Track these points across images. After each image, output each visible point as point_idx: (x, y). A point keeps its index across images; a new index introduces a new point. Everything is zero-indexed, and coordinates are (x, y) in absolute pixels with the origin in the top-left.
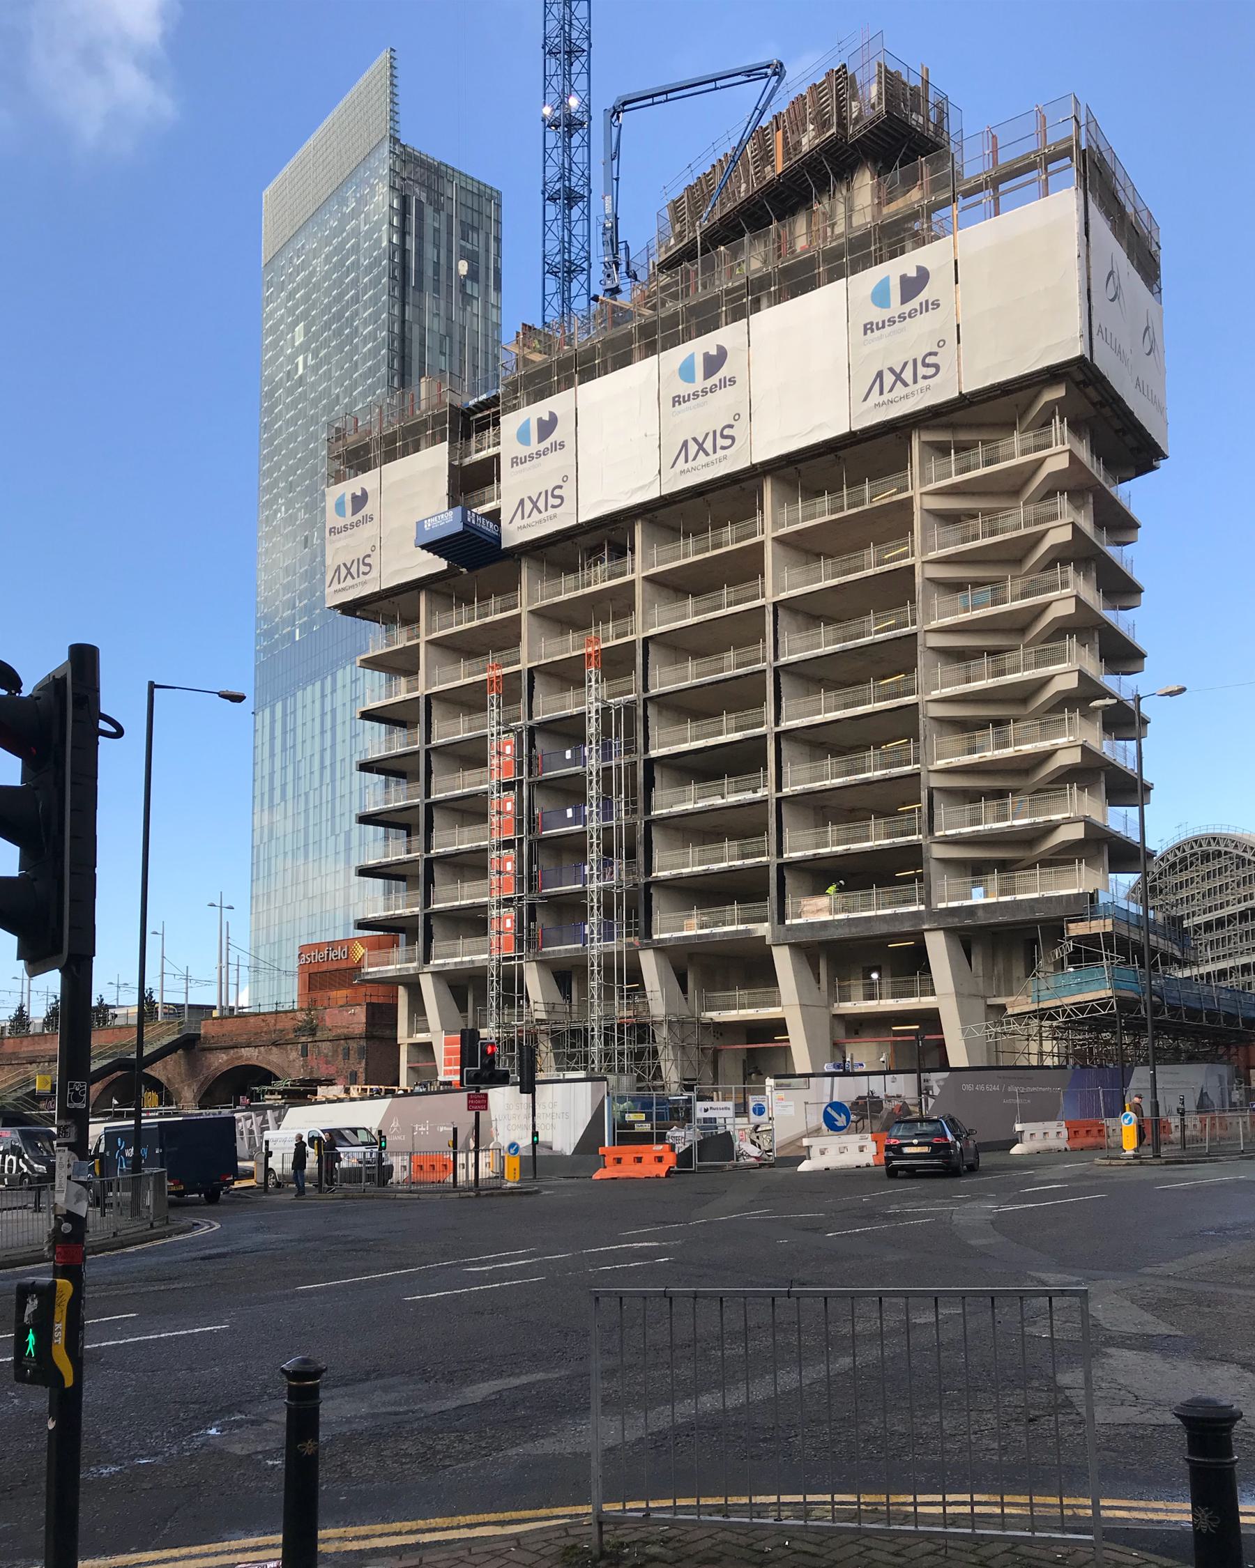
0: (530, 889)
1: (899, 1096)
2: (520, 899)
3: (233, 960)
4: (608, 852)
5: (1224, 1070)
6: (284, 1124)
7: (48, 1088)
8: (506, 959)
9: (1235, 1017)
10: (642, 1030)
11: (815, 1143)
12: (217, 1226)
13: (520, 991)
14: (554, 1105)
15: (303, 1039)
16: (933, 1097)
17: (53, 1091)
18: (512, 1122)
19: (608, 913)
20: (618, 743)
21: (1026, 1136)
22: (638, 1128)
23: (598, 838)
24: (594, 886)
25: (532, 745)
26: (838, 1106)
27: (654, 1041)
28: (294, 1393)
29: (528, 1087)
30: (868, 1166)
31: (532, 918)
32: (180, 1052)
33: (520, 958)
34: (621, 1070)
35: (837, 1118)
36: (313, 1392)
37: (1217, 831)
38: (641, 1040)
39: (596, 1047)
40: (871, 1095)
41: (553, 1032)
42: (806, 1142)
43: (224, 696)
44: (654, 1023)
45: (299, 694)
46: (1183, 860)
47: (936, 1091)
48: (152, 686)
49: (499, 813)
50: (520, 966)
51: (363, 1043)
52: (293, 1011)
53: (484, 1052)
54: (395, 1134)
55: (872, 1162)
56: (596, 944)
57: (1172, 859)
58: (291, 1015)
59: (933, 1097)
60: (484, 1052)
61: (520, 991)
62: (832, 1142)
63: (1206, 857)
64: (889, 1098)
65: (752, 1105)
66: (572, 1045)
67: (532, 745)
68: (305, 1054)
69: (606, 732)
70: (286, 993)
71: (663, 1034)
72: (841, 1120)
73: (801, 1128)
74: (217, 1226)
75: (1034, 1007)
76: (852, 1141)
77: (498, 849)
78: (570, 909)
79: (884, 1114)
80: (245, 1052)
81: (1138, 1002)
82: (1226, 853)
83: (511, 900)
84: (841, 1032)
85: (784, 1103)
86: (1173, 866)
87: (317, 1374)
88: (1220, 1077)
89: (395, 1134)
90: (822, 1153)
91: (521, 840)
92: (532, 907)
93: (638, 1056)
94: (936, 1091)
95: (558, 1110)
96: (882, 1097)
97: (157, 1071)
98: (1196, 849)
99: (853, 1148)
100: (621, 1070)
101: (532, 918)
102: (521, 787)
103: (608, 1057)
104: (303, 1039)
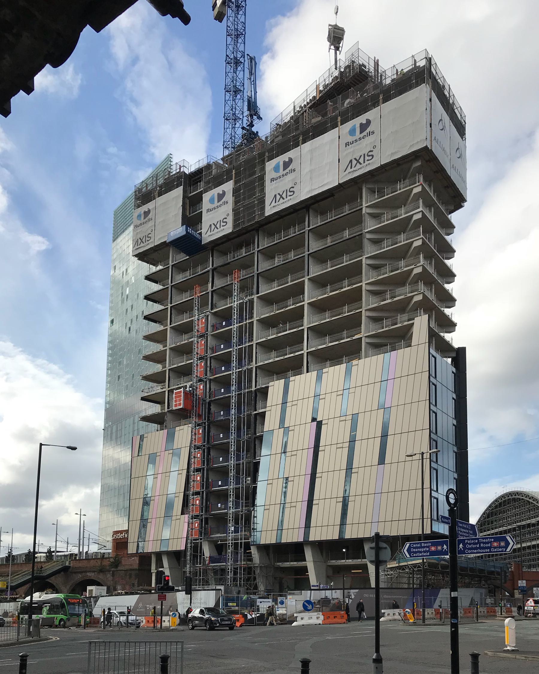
0: (206, 511)
1: (337, 598)
2: (202, 515)
3: (86, 535)
4: (237, 497)
5: (483, 591)
6: (98, 603)
7: (5, 587)
8: (194, 540)
9: (484, 570)
10: (249, 570)
11: (299, 616)
12: (58, 639)
13: (201, 552)
14: (201, 599)
15: (113, 569)
16: (351, 599)
17: (7, 588)
18: (185, 605)
19: (237, 522)
20: (243, 454)
21: (386, 614)
22: (233, 608)
23: (233, 492)
24: (231, 511)
25: (209, 454)
26: (309, 602)
27: (254, 574)
28: (21, 660)
29: (189, 592)
30: (320, 624)
31: (207, 523)
32: (62, 573)
33: (201, 539)
34: (240, 585)
35: (308, 606)
36: (26, 660)
37: (519, 490)
38: (249, 573)
39: (230, 576)
40: (326, 598)
41: (214, 569)
42: (295, 615)
43: (68, 447)
44: (254, 567)
45: (123, 422)
46: (505, 501)
47: (353, 597)
48: (41, 445)
49: (194, 481)
50: (201, 543)
51: (137, 572)
52: (109, 558)
53: (165, 579)
54: (141, 608)
55: (321, 623)
56: (231, 534)
57: (500, 501)
58: (108, 560)
59: (351, 599)
60: (165, 579)
61: (201, 552)
62: (306, 615)
63: (514, 499)
64: (333, 599)
65: (279, 600)
66: (220, 575)
67: (209, 454)
68: (113, 575)
69: (238, 450)
70: (109, 549)
71: (258, 571)
72: (310, 607)
73: (294, 610)
74: (58, 639)
75: (397, 565)
76: (314, 615)
77: (193, 495)
78: (222, 520)
79: (331, 605)
80: (89, 574)
81: (438, 564)
82: (523, 499)
83: (198, 516)
84: (331, 573)
85: (292, 600)
86: (500, 504)
87: (27, 656)
88: (481, 594)
89: (141, 608)
90: (302, 619)
91: (203, 492)
92: (207, 519)
93: (248, 579)
94: (353, 597)
95: (202, 601)
96: (331, 598)
97: (52, 580)
98: (510, 497)
99: (314, 618)
100: (240, 585)
101: (207, 523)
102: (204, 470)
103: (235, 580)
104: (113, 569)
